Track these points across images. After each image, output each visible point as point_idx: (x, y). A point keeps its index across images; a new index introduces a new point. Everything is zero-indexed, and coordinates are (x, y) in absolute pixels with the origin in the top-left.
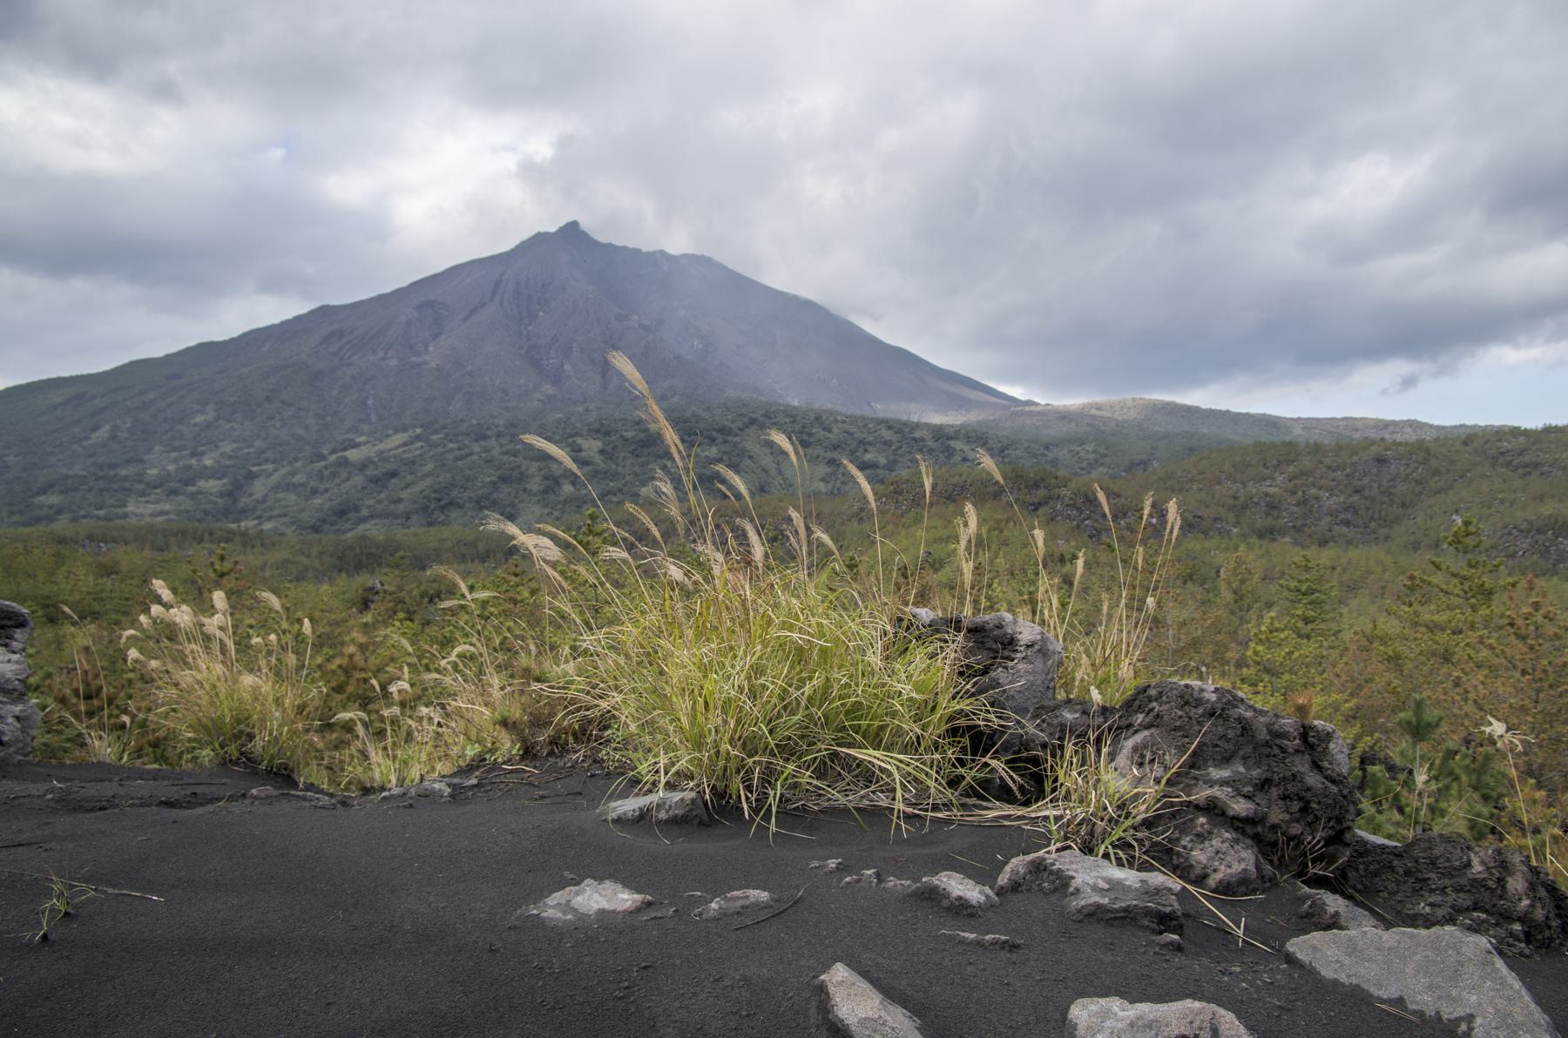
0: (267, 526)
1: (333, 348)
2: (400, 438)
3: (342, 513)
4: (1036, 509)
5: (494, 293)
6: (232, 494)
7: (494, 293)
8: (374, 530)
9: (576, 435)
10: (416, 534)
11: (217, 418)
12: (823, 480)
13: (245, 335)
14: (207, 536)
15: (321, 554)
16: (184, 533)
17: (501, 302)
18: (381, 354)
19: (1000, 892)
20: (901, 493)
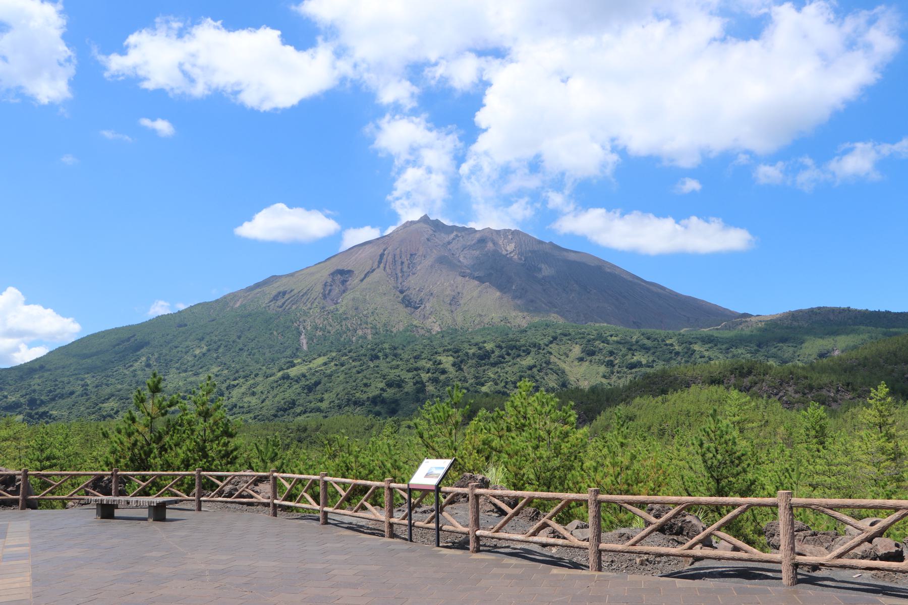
1: (279, 303)
2: (321, 360)
5: (380, 262)
7: (380, 262)
11: (209, 350)
12: (604, 377)
17: (385, 268)
18: (309, 305)
19: (109, 99)
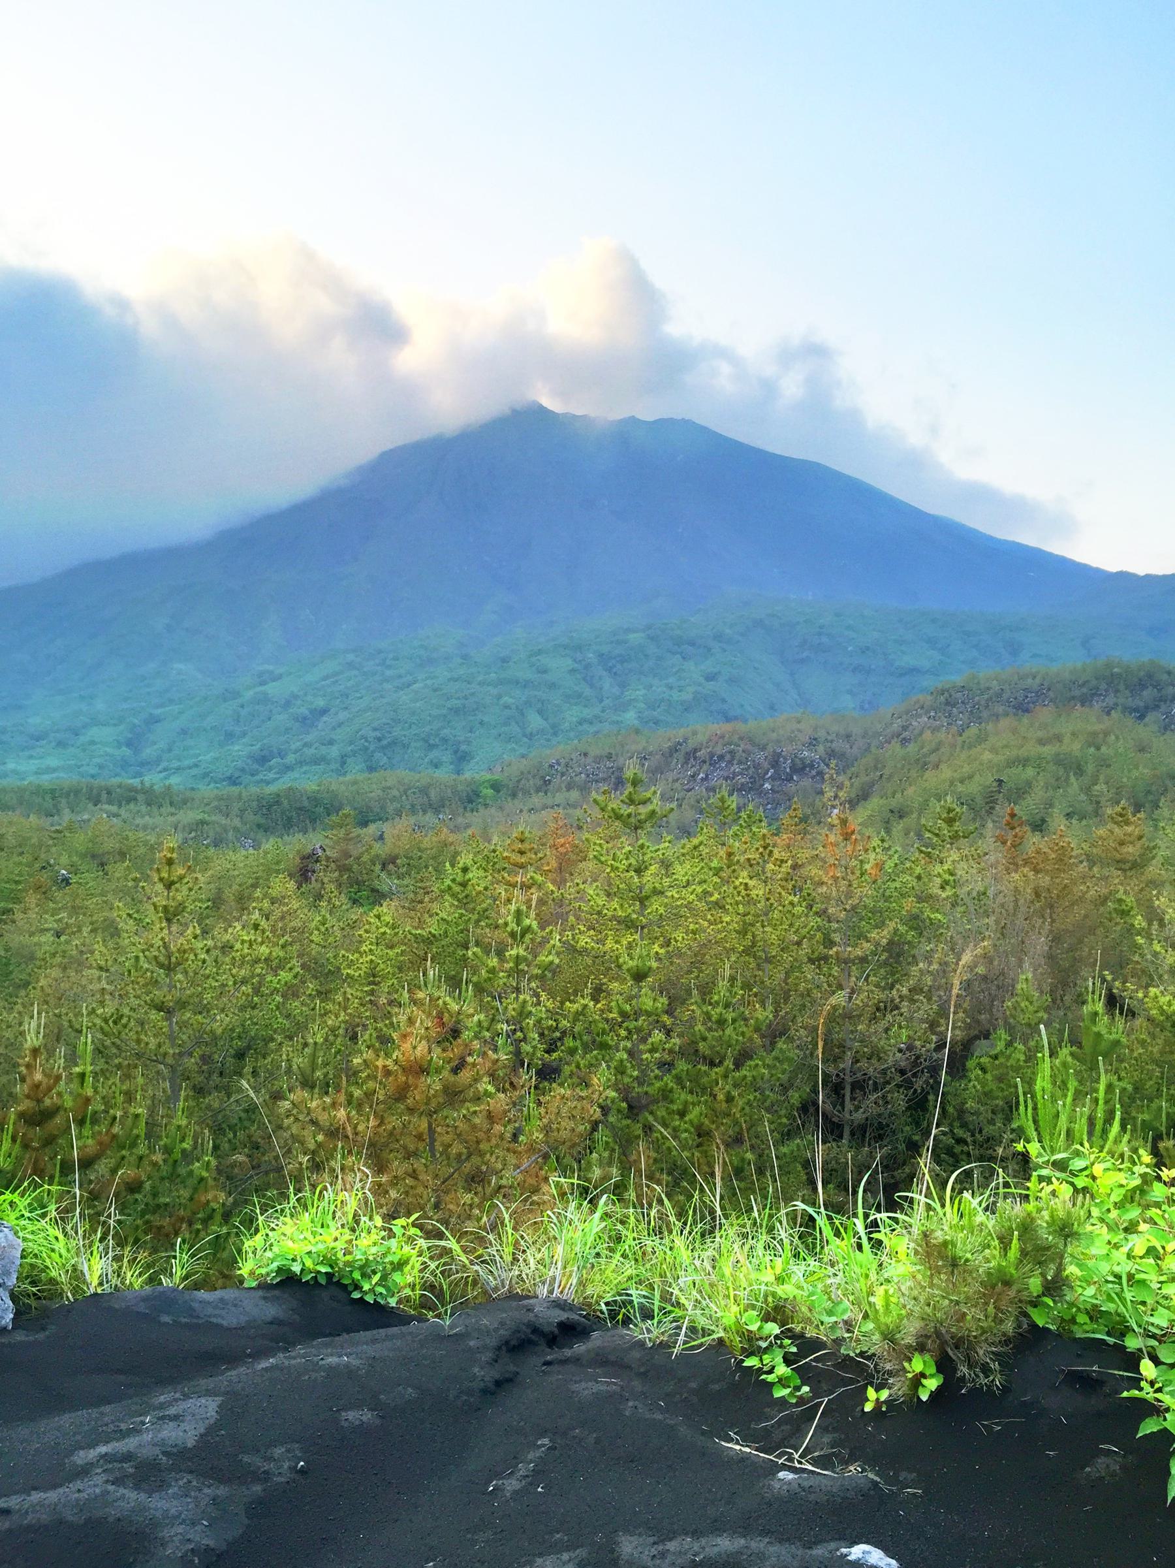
0: (174, 780)
3: (263, 759)
4: (1141, 717)
6: (133, 742)
8: (307, 782)
9: (540, 652)
10: (355, 783)
12: (850, 692)
13: (804, 463)
14: (104, 796)
15: (242, 811)
16: (77, 792)
20: (954, 706)
